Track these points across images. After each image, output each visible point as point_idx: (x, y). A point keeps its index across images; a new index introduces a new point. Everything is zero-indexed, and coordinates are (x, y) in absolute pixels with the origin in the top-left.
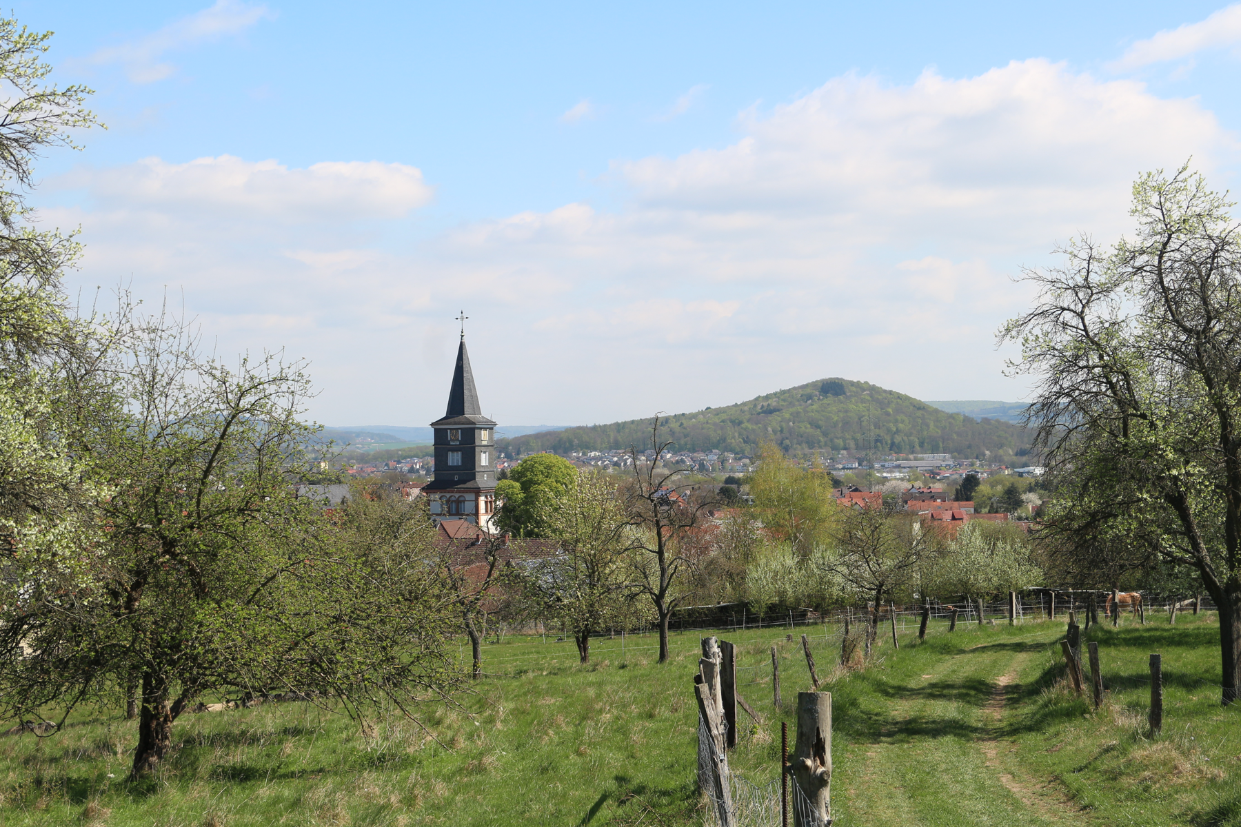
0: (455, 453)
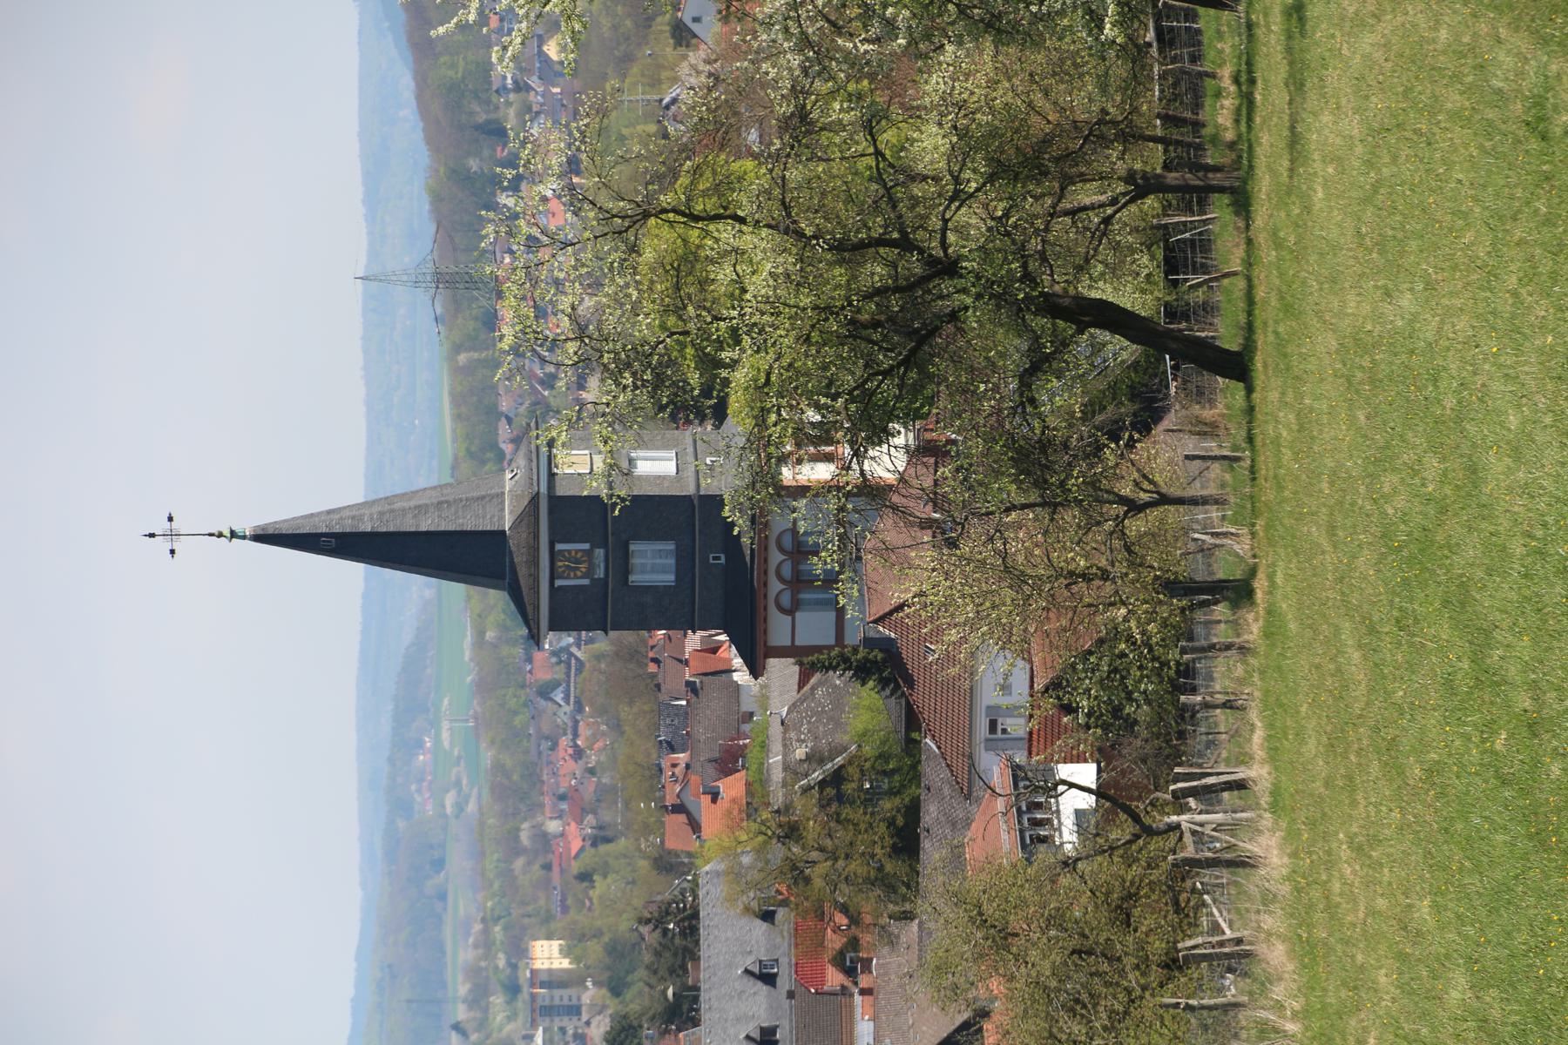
0: (636, 561)
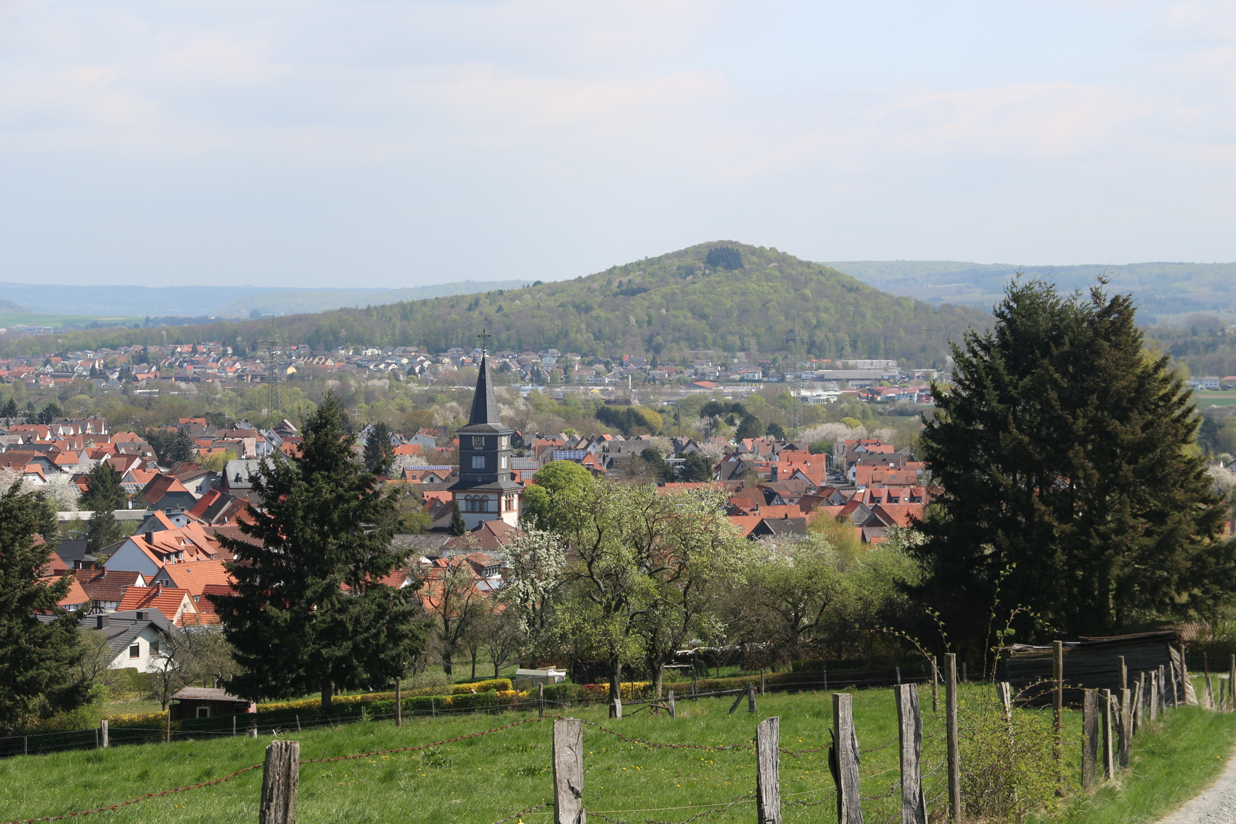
0: (479, 458)
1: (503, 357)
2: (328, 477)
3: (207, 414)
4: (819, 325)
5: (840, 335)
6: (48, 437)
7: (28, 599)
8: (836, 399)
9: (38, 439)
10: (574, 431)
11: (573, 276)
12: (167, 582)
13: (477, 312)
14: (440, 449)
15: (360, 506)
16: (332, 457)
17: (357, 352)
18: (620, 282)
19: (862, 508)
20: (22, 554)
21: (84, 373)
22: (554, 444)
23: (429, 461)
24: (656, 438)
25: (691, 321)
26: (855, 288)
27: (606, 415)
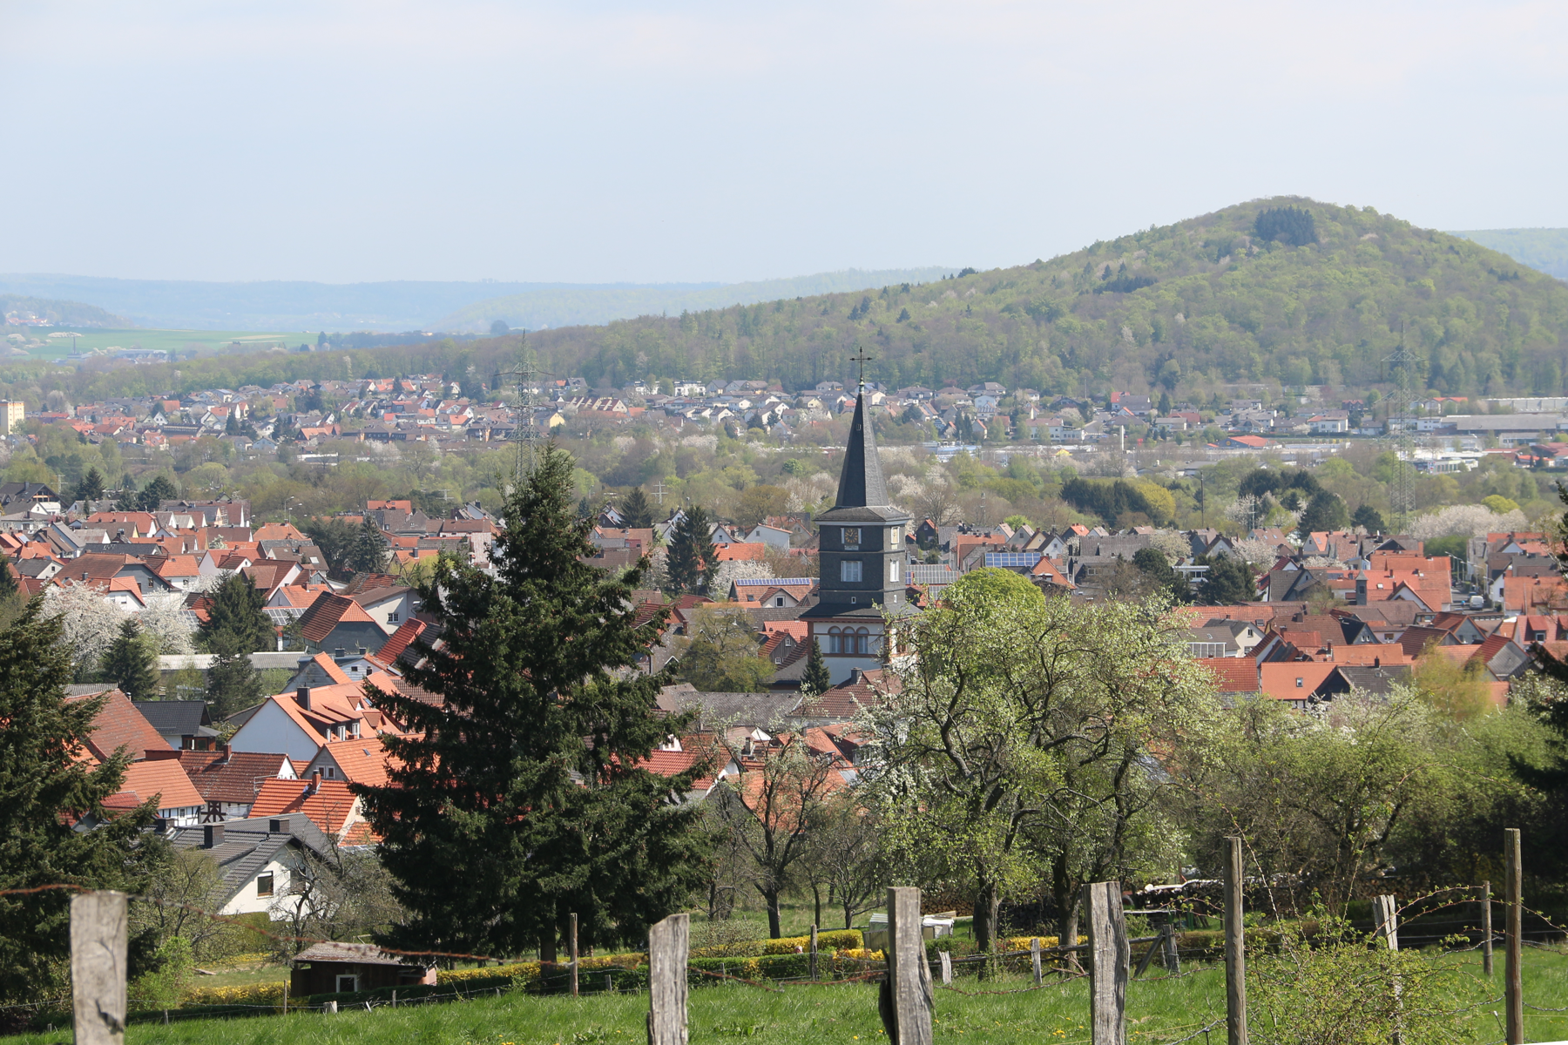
0: (852, 564)
1: (909, 396)
2: (550, 589)
3: (414, 493)
4: (1449, 338)
5: (1484, 355)
6: (153, 531)
7: (54, 794)
8: (1476, 464)
9: (135, 535)
10: (1024, 519)
11: (1026, 260)
12: (331, 770)
13: (865, 322)
14: (795, 550)
15: (602, 638)
16: (556, 555)
17: (665, 390)
18: (1107, 268)
19: (1510, 648)
20: (44, 719)
21: (218, 427)
22: (988, 541)
23: (776, 571)
24: (1161, 532)
25: (1227, 334)
26: (1511, 274)
27: (1078, 494)
